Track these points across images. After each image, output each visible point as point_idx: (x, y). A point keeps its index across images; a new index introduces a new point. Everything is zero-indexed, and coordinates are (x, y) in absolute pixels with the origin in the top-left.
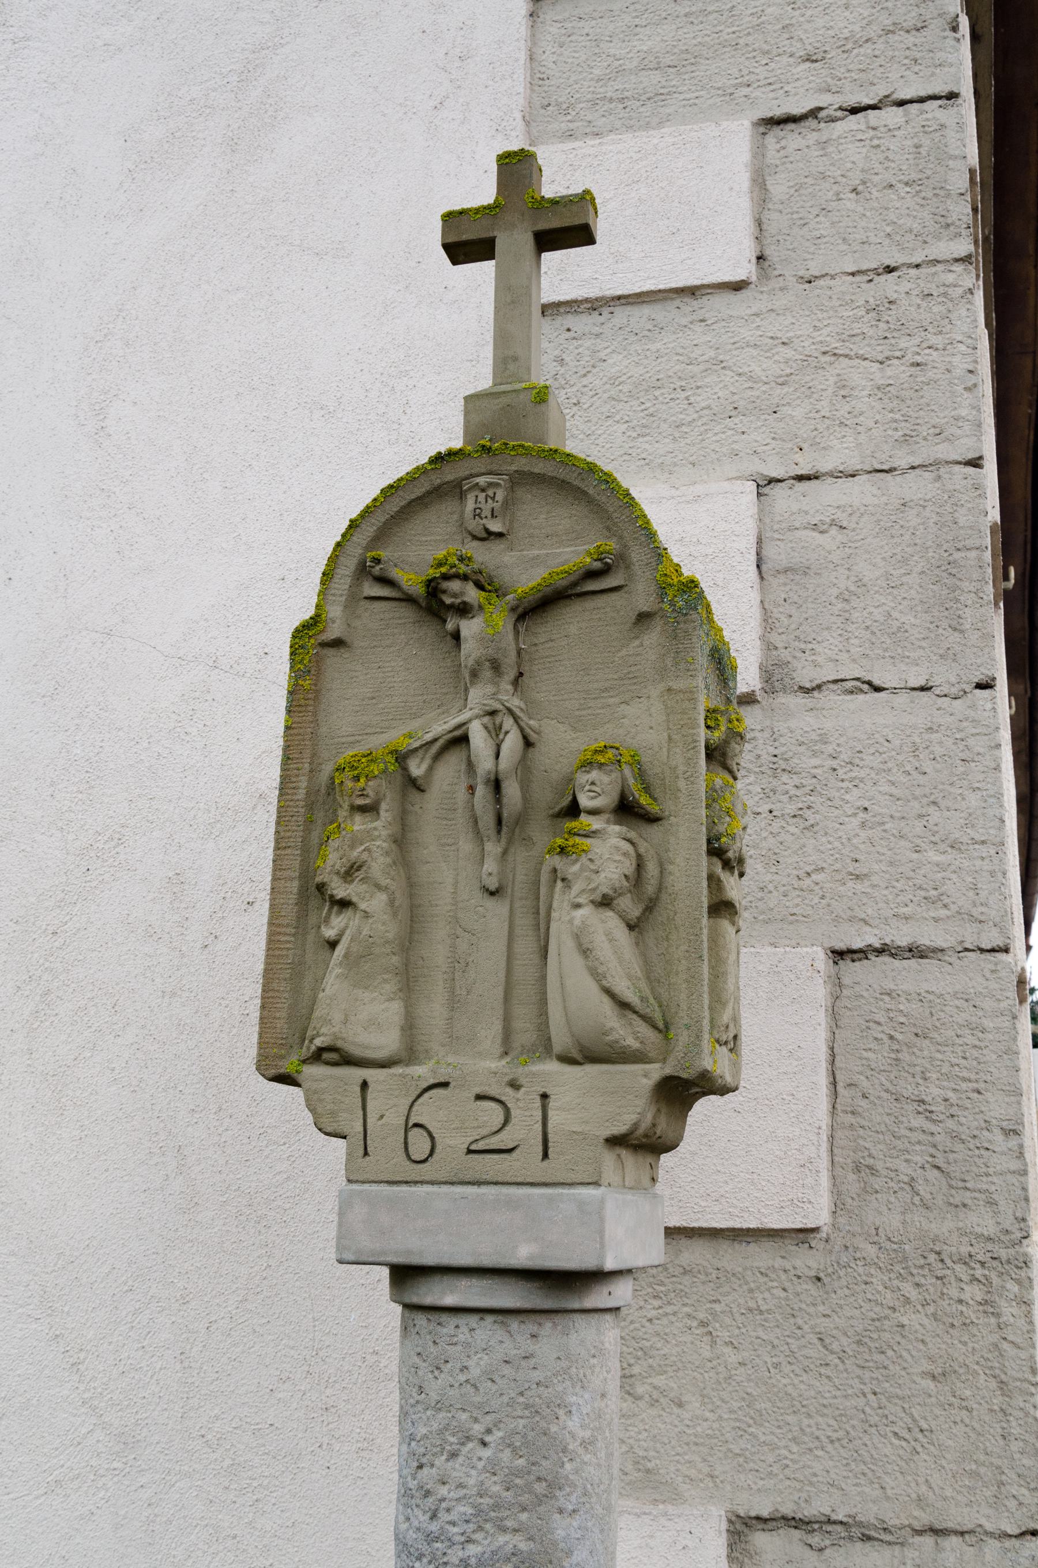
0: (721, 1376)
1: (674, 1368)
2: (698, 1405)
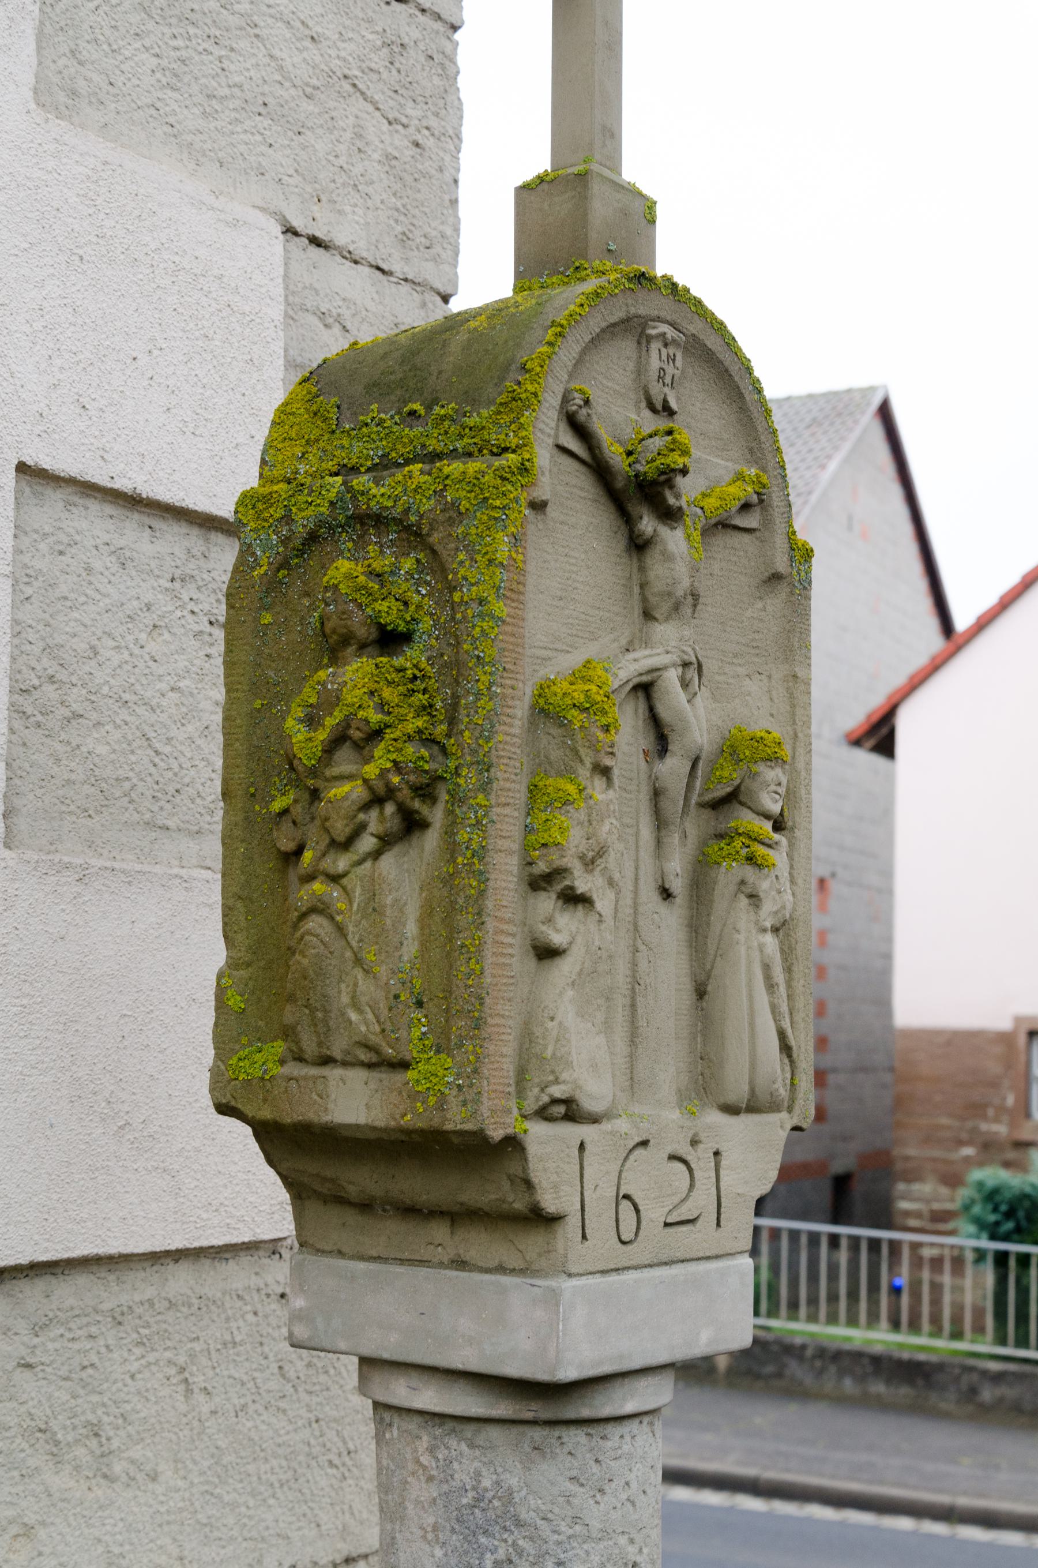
0: (195, 1432)
1: (152, 1432)
2: (170, 1473)
